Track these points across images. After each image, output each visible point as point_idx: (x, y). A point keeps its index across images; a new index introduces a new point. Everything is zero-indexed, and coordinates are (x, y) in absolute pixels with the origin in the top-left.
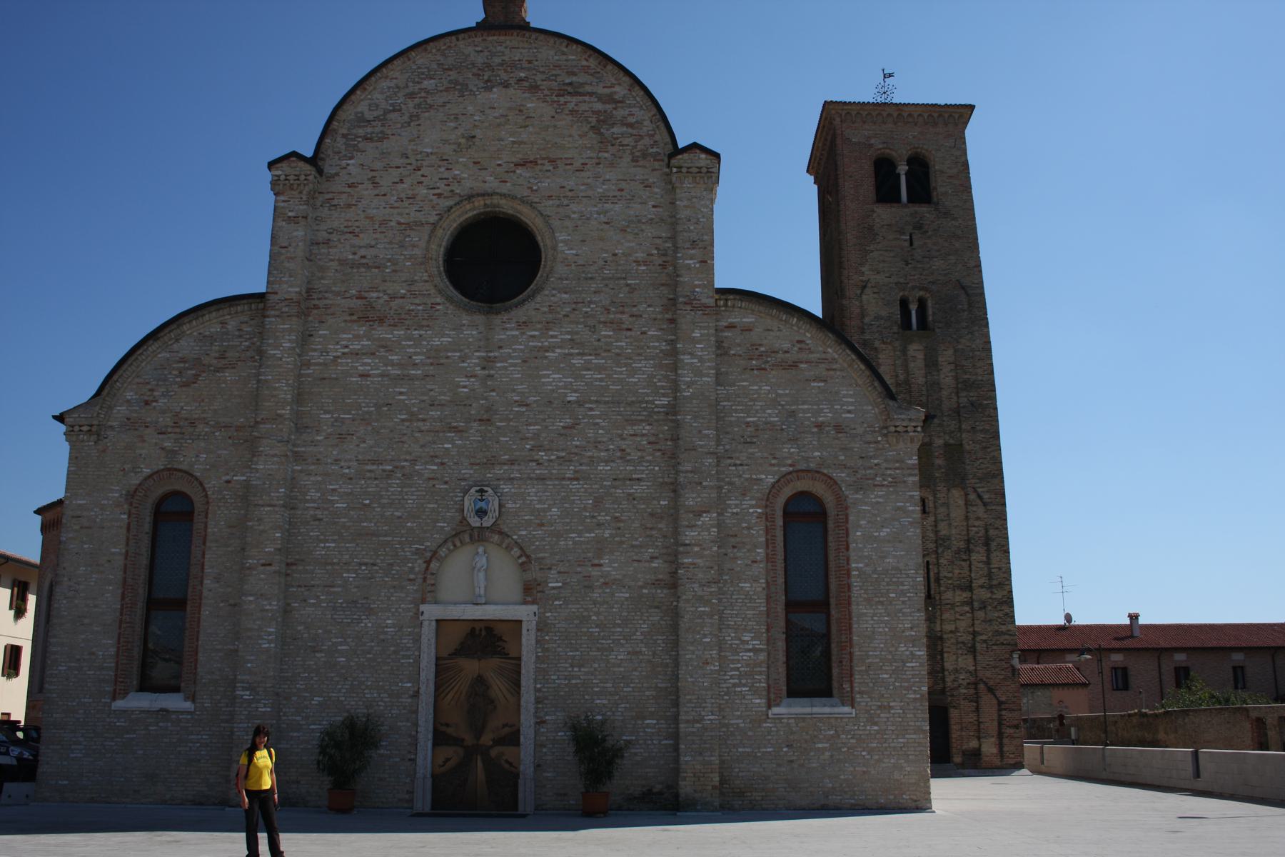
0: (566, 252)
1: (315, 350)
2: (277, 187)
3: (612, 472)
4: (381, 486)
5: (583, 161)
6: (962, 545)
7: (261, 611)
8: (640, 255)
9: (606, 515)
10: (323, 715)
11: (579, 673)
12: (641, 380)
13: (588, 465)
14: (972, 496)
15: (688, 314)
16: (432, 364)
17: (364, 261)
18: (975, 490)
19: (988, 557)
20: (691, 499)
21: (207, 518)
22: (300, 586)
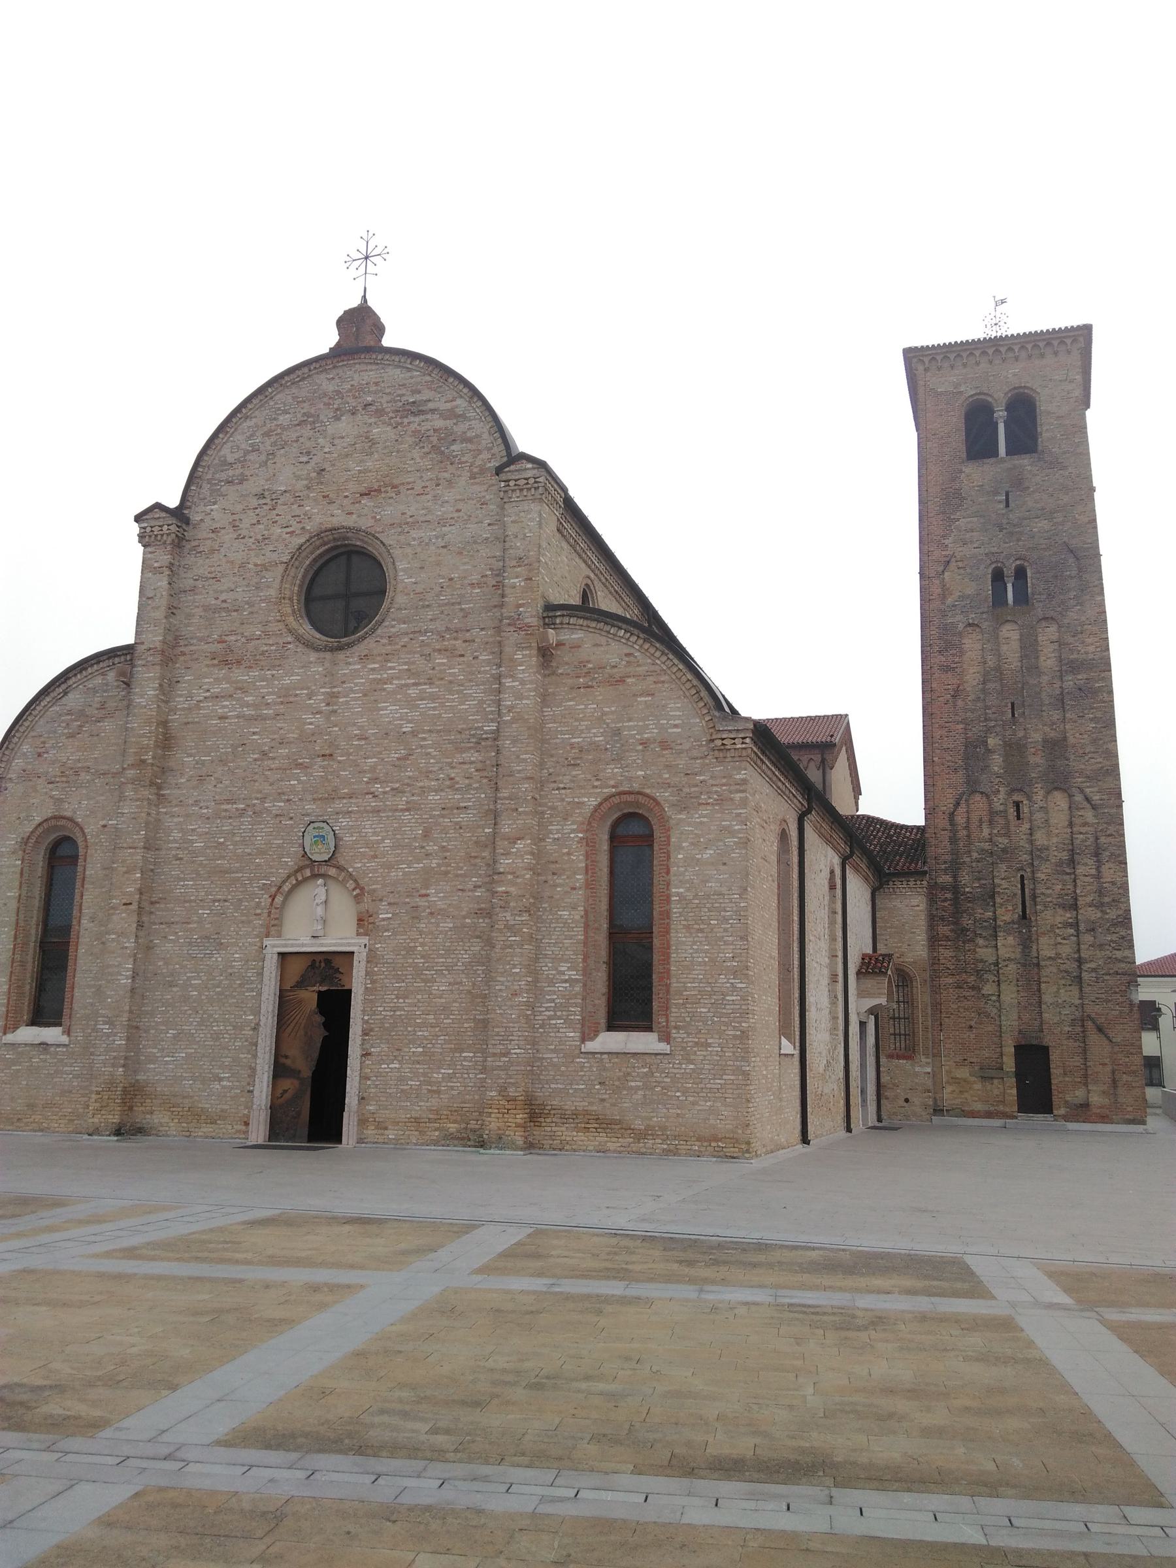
0: (406, 580)
1: (181, 696)
2: (144, 538)
3: (441, 801)
4: (235, 824)
5: (423, 484)
6: (1065, 856)
7: (122, 948)
8: (475, 578)
9: (434, 845)
10: (176, 1047)
11: (404, 1005)
12: (472, 706)
13: (419, 795)
14: (1079, 798)
15: (512, 635)
16: (282, 703)
17: (224, 605)
18: (1082, 791)
19: (1098, 869)
20: (507, 827)
21: (85, 861)
22: (162, 923)
